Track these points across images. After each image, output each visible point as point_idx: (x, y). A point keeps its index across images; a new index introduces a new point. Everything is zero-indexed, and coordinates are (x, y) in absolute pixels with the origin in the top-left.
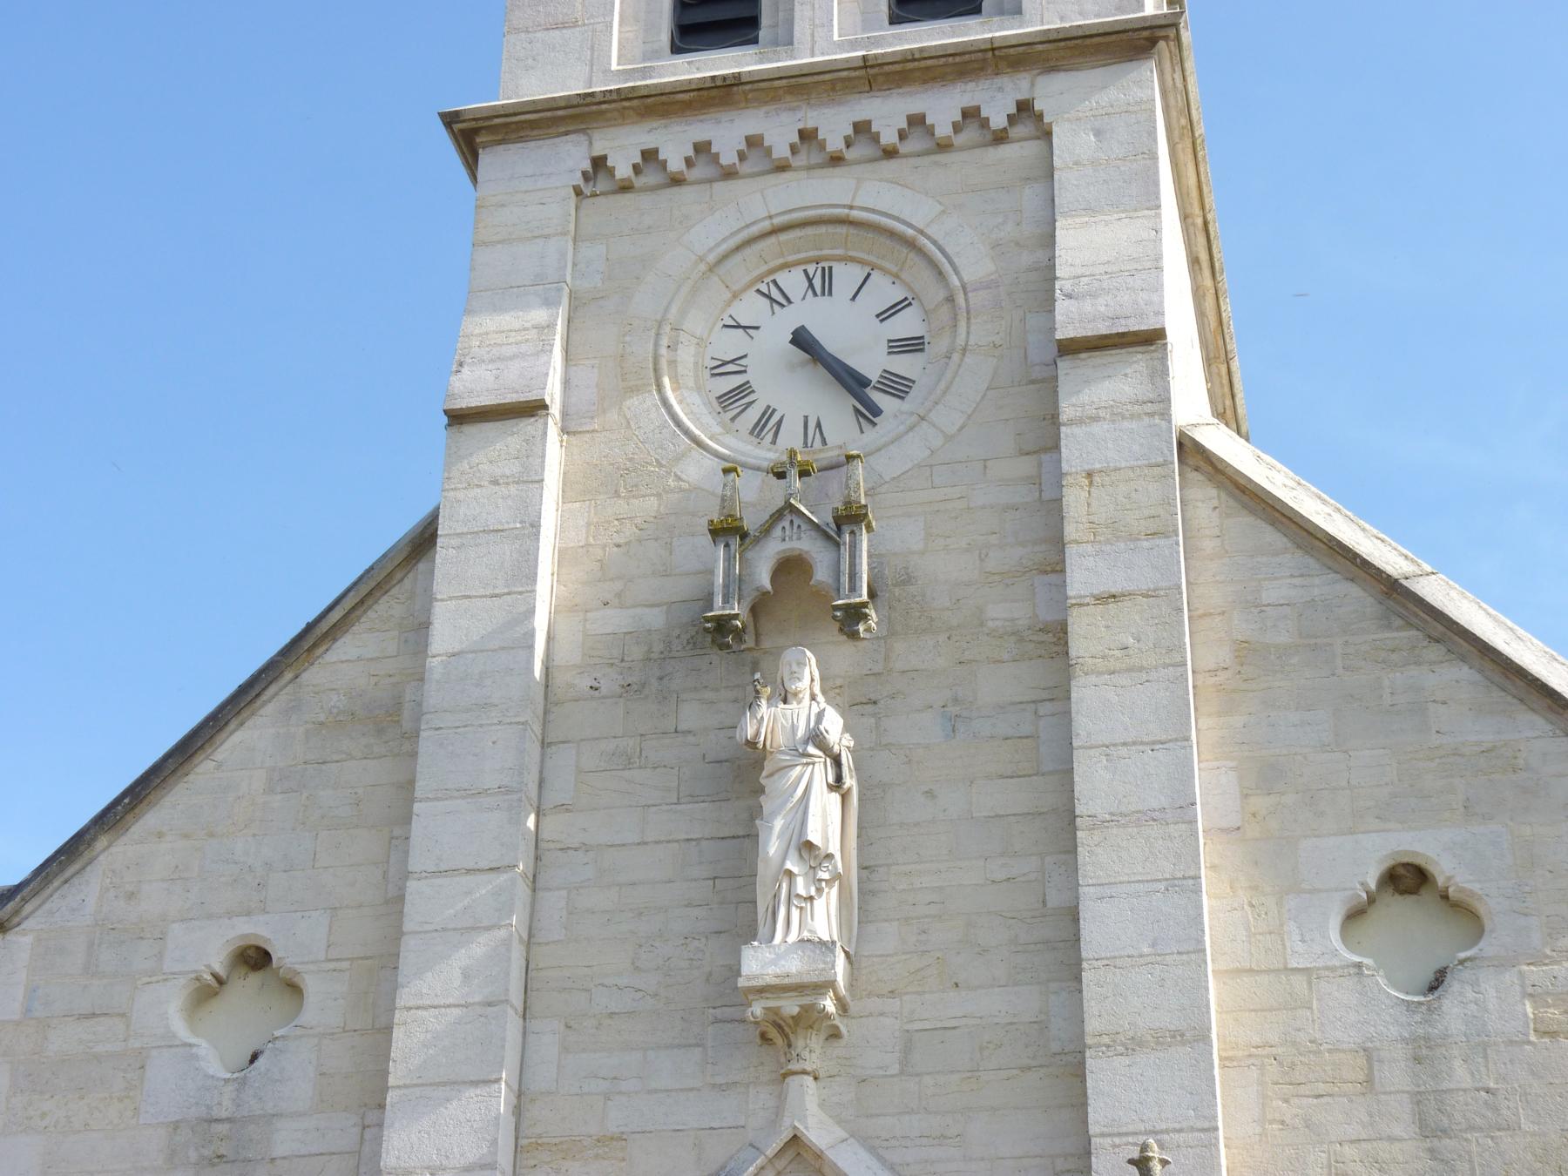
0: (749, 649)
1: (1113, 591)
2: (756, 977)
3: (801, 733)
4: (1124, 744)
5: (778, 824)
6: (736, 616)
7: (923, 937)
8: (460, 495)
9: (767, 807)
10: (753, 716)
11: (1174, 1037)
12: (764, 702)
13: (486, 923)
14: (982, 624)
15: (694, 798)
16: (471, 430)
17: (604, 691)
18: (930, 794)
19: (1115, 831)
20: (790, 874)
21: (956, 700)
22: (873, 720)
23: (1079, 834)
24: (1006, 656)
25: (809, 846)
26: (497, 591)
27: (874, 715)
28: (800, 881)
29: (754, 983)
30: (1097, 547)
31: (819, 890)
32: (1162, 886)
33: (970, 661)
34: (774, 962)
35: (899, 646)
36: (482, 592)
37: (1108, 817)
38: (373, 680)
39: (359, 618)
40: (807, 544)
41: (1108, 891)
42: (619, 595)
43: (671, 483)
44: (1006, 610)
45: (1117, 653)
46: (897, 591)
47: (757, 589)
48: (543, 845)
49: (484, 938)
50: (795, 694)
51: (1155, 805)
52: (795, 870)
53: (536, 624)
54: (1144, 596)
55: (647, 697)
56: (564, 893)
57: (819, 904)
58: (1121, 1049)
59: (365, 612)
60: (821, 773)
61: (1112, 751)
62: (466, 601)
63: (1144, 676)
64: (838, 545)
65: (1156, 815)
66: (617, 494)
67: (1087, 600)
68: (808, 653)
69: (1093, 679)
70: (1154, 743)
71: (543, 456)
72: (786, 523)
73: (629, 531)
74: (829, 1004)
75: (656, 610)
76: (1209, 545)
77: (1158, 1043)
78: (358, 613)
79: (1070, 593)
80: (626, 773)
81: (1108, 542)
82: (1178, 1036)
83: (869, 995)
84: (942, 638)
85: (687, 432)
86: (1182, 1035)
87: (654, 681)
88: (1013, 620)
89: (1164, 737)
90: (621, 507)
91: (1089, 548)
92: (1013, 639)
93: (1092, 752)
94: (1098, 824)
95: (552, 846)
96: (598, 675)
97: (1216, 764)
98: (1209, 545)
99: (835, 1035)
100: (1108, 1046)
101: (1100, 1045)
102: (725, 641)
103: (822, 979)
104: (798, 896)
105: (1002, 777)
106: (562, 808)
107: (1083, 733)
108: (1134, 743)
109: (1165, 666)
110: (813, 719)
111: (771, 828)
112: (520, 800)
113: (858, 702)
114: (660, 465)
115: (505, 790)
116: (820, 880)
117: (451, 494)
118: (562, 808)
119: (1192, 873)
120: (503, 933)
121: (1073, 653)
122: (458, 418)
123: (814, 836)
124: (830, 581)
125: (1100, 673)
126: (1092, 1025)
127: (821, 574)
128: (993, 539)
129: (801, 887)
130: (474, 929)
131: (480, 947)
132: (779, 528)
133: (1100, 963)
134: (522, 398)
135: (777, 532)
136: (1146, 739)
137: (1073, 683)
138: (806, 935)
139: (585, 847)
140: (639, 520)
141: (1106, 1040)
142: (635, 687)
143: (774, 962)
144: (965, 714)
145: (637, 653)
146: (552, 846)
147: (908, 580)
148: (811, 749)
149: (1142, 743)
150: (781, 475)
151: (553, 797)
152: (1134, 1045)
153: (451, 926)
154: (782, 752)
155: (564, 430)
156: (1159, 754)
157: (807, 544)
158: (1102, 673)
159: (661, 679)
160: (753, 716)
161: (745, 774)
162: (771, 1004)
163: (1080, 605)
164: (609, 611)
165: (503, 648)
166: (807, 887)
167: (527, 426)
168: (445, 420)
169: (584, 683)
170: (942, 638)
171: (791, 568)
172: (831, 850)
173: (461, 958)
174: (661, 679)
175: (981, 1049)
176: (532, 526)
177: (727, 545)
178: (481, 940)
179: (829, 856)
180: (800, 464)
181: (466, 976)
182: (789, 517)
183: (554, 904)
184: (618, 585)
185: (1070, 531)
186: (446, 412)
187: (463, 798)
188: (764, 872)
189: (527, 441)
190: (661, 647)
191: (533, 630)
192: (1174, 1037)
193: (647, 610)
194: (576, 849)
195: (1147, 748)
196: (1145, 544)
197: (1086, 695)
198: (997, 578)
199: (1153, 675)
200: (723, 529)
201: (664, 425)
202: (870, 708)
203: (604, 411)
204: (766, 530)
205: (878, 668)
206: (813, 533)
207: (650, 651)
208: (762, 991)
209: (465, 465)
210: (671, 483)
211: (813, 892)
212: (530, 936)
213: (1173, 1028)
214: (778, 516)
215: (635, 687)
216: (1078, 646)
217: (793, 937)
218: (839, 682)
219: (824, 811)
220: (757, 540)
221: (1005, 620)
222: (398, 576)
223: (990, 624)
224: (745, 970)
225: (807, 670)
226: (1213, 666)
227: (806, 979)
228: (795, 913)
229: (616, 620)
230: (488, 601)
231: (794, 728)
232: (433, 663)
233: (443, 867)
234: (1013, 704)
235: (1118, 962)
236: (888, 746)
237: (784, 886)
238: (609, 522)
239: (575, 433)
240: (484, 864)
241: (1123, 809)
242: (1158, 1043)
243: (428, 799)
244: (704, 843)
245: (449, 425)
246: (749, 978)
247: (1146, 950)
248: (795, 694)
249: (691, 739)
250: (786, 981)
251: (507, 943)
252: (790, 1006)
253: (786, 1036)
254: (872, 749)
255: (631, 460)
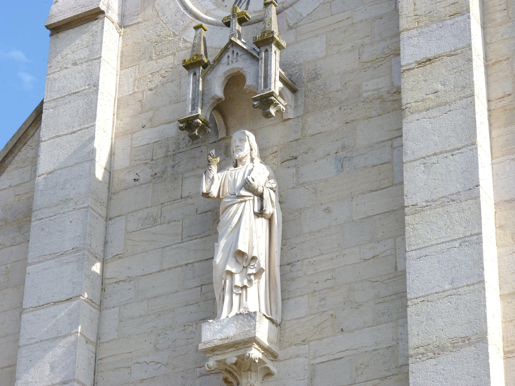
0: (224, 139)
1: (429, 56)
2: (209, 342)
3: (239, 183)
4: (435, 154)
5: (222, 243)
6: (197, 117)
7: (323, 303)
8: (56, 76)
9: (220, 231)
10: (207, 177)
11: (464, 341)
12: (214, 168)
13: (64, 333)
14: (359, 96)
15: (191, 237)
16: (62, 35)
17: (141, 181)
18: (328, 210)
19: (428, 212)
20: (231, 274)
21: (344, 148)
22: (294, 170)
23: (407, 218)
24: (374, 113)
25: (240, 254)
26: (74, 130)
27: (295, 166)
28: (237, 277)
29: (208, 346)
30: (419, 30)
31: (250, 281)
32: (457, 245)
33: (352, 121)
34: (220, 331)
35: (310, 119)
36: (66, 132)
37: (424, 204)
38: (17, 198)
39: (10, 163)
40: (242, 64)
41: (424, 252)
42: (151, 120)
43: (181, 45)
44: (373, 84)
45: (431, 96)
46: (309, 85)
47: (213, 98)
48: (106, 282)
49: (62, 343)
50: (241, 160)
51: (453, 190)
52: (234, 270)
53: (97, 144)
54: (448, 56)
55: (165, 180)
56: (117, 309)
57: (252, 291)
58: (431, 355)
59: (14, 158)
60: (251, 205)
61: (428, 161)
62: (58, 139)
63: (448, 108)
64: (258, 60)
65: (454, 197)
66: (151, 58)
67: (413, 66)
68: (247, 133)
69: (416, 116)
70: (453, 150)
71: (101, 43)
72: (230, 53)
73: (157, 79)
74: (255, 353)
75: (171, 125)
76: (499, 16)
77: (453, 347)
78: (10, 159)
79: (403, 63)
80: (153, 229)
81: (427, 26)
82: (466, 340)
83: (290, 345)
84: (336, 109)
85: (191, 12)
86: (469, 340)
87: (169, 169)
88: (378, 89)
89: (459, 145)
90: (153, 65)
91: (414, 32)
92: (379, 101)
93: (415, 163)
94: (418, 210)
95: (111, 281)
96: (138, 171)
97: (504, 158)
98: (499, 16)
99: (269, 374)
100: (423, 354)
101: (418, 354)
102: (204, 134)
103: (247, 337)
104: (236, 287)
105: (371, 191)
106: (118, 257)
107: (409, 152)
108: (441, 153)
109: (461, 99)
110: (247, 173)
111: (218, 246)
112: (84, 255)
113: (283, 160)
114: (175, 35)
115: (76, 250)
116: (250, 275)
117: (51, 76)
118: (118, 257)
119: (476, 231)
120: (72, 338)
121: (404, 102)
122: (56, 29)
123: (243, 247)
124: (255, 84)
125: (420, 111)
126: (413, 341)
127: (249, 81)
128: (367, 40)
129: (238, 281)
130: (57, 338)
131: (59, 349)
132: (226, 57)
133: (418, 300)
134: (87, 9)
135: (225, 60)
136: (448, 149)
137: (404, 121)
138: (242, 310)
139: (129, 279)
140: (163, 72)
141: (422, 350)
142: (159, 175)
143: (220, 331)
144: (349, 155)
145: (160, 153)
146: (111, 281)
147: (315, 77)
148: (243, 192)
149: (446, 152)
150: (228, 24)
151: (114, 249)
152: (439, 350)
153: (46, 338)
154: (227, 197)
155: (122, 25)
156: (456, 157)
157: (242, 64)
158: (422, 111)
159: (173, 167)
160: (207, 177)
161: (211, 215)
162: (220, 358)
163: (409, 70)
164: (145, 131)
165: (76, 164)
166: (242, 280)
167: (93, 26)
168: (49, 32)
169: (130, 177)
170: (336, 109)
171: (234, 81)
172: (255, 254)
173: (49, 357)
174: (173, 167)
175: (357, 369)
176: (94, 86)
177: (195, 74)
178: (61, 344)
179: (254, 258)
180: (239, 14)
181: (52, 368)
182: (231, 49)
183: (111, 316)
184: (151, 114)
185: (403, 23)
186: (47, 27)
187: (53, 258)
188: (216, 274)
189: (93, 36)
190: (174, 146)
191: (93, 151)
192: (464, 341)
193: (166, 126)
194: (124, 281)
195: (449, 154)
196: (449, 22)
197: (411, 126)
198: (369, 65)
199: (453, 106)
200: (191, 64)
201: (178, 10)
202: (293, 162)
203: (145, 9)
204: (218, 60)
205: (298, 136)
206: (245, 56)
207: (168, 151)
208: (214, 350)
209: (59, 57)
210: (181, 45)
211: (246, 283)
212: (98, 338)
213: (463, 335)
214: (226, 49)
215: (159, 175)
216: (408, 97)
217: (233, 313)
218: (275, 149)
219: (251, 229)
220: (213, 67)
221: (373, 90)
222: (31, 133)
223: (365, 95)
224: (204, 339)
225: (247, 144)
226: (501, 95)
227: (238, 338)
228: (236, 298)
229: (148, 136)
230: (69, 137)
231: (235, 181)
232: (39, 180)
233: (41, 303)
234: (378, 143)
235: (430, 298)
236: (303, 184)
237: (228, 282)
238: (146, 76)
239: (128, 26)
240: (64, 297)
241: (434, 197)
242: (453, 347)
243: (35, 263)
244: (196, 264)
245: (51, 35)
246: (205, 344)
247: (447, 287)
248: (241, 160)
249: (190, 201)
250: (226, 341)
251: (75, 344)
252: (231, 358)
253: (236, 378)
254: (293, 188)
255: (159, 36)
